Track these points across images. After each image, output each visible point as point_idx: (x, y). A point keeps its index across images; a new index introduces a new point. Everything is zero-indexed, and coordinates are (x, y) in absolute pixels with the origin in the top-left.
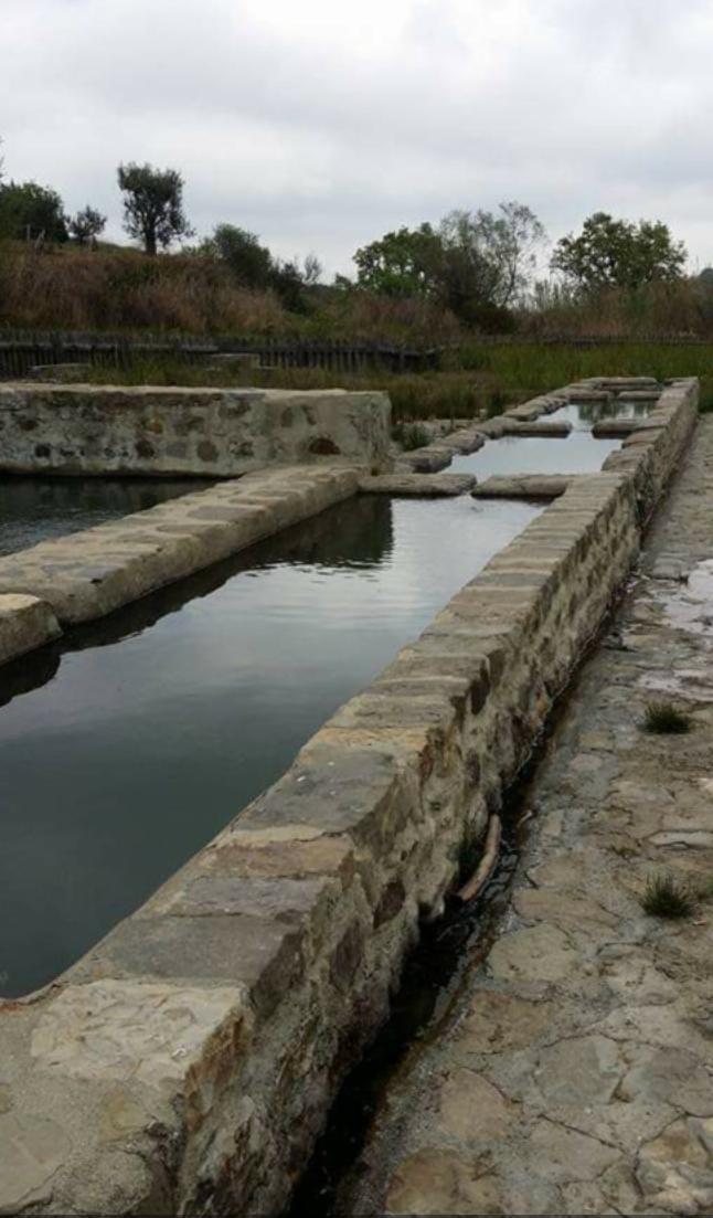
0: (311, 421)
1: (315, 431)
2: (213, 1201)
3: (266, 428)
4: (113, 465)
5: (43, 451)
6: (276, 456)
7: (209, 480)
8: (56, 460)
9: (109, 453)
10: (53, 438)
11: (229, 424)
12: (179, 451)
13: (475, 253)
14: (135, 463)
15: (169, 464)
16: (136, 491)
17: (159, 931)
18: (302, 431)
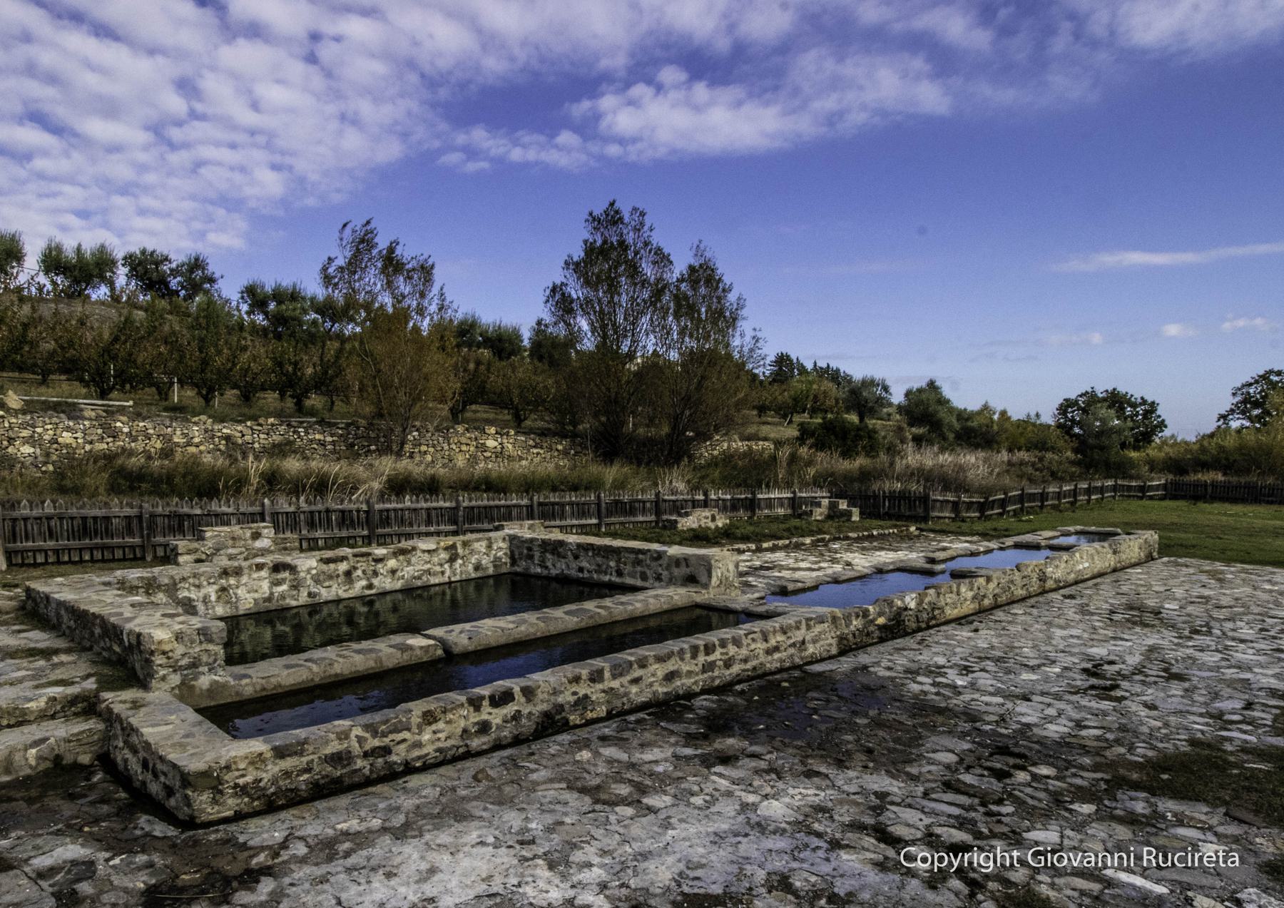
0: (687, 566)
1: (688, 571)
2: (1242, 427)
3: (668, 568)
4: (607, 578)
5: (581, 570)
6: (671, 582)
7: (634, 589)
8: (586, 575)
9: (606, 573)
10: (585, 564)
11: (654, 564)
12: (632, 575)
13: (729, 736)
14: (615, 579)
15: (629, 581)
16: (574, 589)
17: (170, 834)
18: (682, 571)
